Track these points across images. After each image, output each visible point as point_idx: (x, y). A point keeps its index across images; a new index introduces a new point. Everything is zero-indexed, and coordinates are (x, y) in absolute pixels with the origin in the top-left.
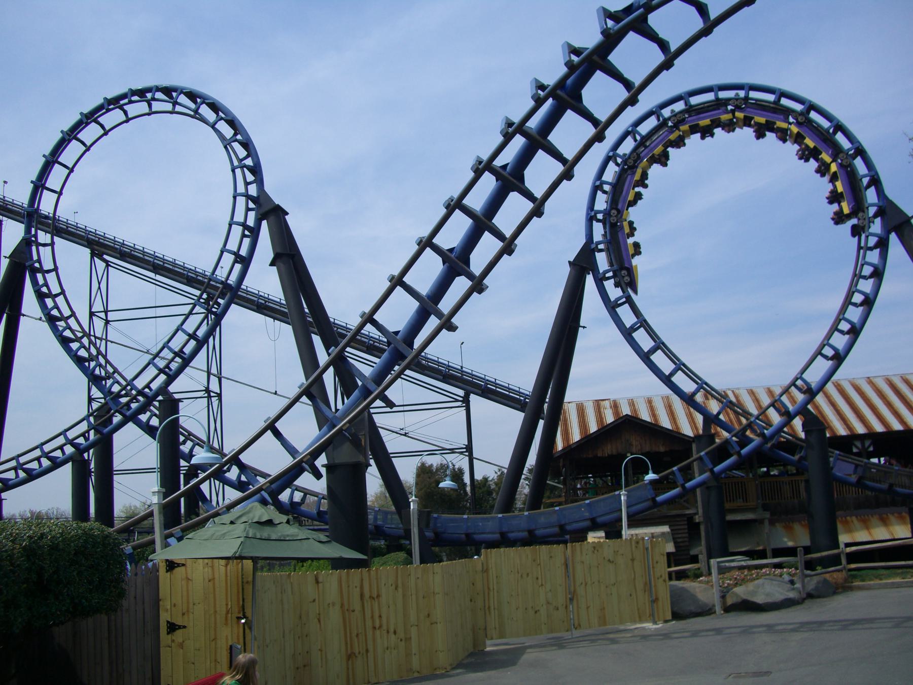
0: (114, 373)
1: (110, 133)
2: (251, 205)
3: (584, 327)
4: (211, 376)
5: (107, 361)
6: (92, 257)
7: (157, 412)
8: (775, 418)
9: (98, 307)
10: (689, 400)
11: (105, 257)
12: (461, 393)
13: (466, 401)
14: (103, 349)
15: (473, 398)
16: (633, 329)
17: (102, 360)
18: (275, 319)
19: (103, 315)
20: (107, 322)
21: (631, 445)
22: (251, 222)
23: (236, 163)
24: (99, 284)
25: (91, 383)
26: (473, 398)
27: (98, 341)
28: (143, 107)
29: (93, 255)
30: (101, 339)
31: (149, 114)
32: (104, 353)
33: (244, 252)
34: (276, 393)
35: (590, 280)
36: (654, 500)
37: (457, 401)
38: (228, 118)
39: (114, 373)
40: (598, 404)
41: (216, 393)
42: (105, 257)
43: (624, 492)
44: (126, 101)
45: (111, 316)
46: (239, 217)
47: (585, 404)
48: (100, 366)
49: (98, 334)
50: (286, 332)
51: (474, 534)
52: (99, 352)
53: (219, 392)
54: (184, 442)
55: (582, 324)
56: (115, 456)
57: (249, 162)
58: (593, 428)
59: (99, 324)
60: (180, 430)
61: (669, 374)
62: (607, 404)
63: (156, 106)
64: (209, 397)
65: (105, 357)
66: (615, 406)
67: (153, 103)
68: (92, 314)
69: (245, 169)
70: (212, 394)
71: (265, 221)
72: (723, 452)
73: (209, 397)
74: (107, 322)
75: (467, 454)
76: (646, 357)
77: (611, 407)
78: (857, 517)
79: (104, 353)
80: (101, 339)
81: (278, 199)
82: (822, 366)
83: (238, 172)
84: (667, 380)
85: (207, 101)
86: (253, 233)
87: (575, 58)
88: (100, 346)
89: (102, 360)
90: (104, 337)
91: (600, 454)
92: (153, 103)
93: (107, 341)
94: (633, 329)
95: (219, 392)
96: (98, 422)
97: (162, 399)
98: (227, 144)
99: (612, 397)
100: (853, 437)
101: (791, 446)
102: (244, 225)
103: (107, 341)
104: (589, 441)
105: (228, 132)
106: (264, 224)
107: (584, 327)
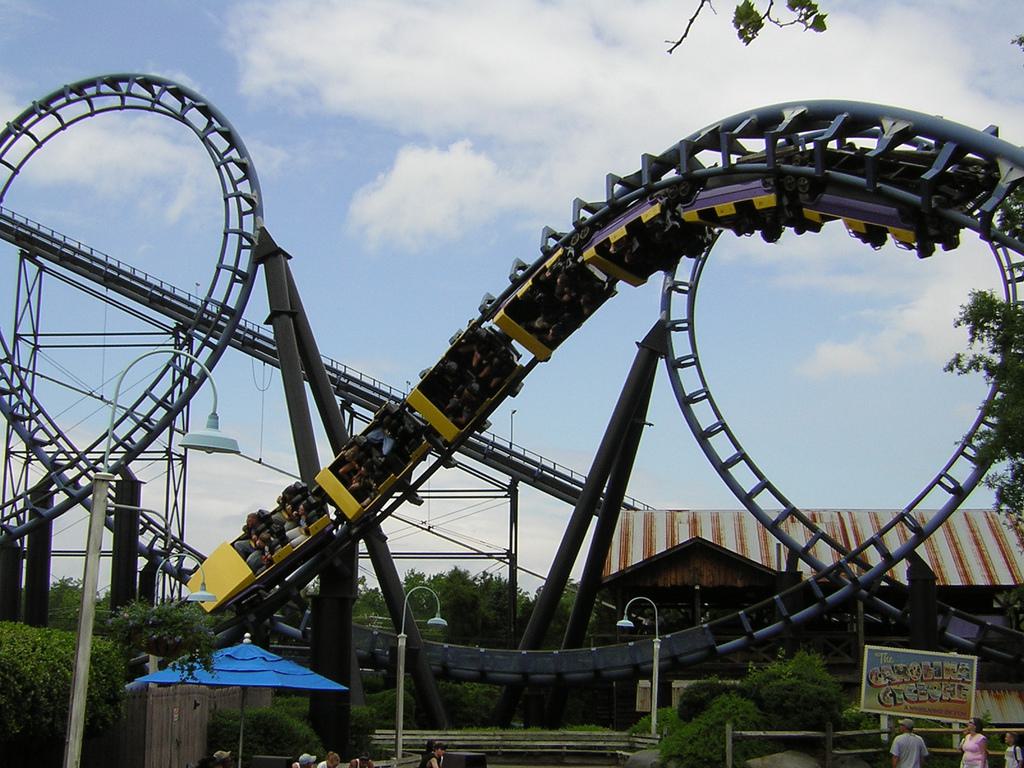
0: (58, 437)
1: (68, 128)
2: (245, 242)
3: (650, 425)
4: (175, 432)
5: (33, 400)
6: (22, 260)
7: (113, 494)
8: (874, 557)
9: (26, 328)
10: (772, 527)
11: (39, 258)
12: (506, 479)
13: (512, 492)
14: (29, 383)
15: (522, 486)
16: (710, 433)
17: (26, 399)
18: (265, 361)
19: (31, 339)
20: (36, 347)
21: (701, 575)
22: (244, 267)
23: (231, 190)
24: (29, 294)
25: (11, 427)
26: (522, 486)
27: (23, 374)
28: (82, 107)
29: (23, 256)
30: (27, 371)
31: (91, 115)
32: (30, 388)
33: (232, 304)
34: (260, 462)
35: (662, 363)
36: (712, 649)
37: (504, 490)
38: (225, 129)
39: (58, 437)
40: (672, 515)
41: (180, 455)
42: (39, 258)
43: (657, 639)
44: (63, 100)
45: (41, 341)
46: (229, 261)
47: (656, 515)
48: (24, 405)
49: (24, 365)
50: (273, 377)
51: (568, 673)
52: (23, 386)
53: (183, 454)
54: (142, 532)
55: (647, 420)
56: (53, 538)
57: (245, 188)
58: (660, 548)
59: (25, 350)
60: (141, 517)
61: (751, 493)
62: (683, 517)
63: (98, 104)
64: (171, 460)
65: (30, 393)
66: (694, 522)
67: (127, 98)
68: (17, 337)
69: (241, 198)
70: (174, 457)
71: (262, 265)
72: (806, 595)
73: (171, 460)
74: (36, 347)
75: (508, 561)
76: (723, 469)
77: (689, 522)
78: (989, 692)
79: (30, 388)
80: (27, 371)
81: (280, 242)
82: (940, 499)
83: (233, 201)
84: (747, 499)
85: (197, 104)
86: (248, 280)
87: (585, 214)
88: (182, 535)
89: (26, 399)
90: (31, 369)
91: (661, 584)
92: (127, 98)
93: (34, 374)
94: (710, 433)
95: (183, 454)
96: (39, 500)
97: (120, 478)
98: (221, 162)
99: (692, 508)
100: (995, 589)
101: (895, 592)
102: (235, 271)
103: (34, 374)
104: (654, 565)
105: (222, 144)
106: (261, 267)
107: (650, 425)
